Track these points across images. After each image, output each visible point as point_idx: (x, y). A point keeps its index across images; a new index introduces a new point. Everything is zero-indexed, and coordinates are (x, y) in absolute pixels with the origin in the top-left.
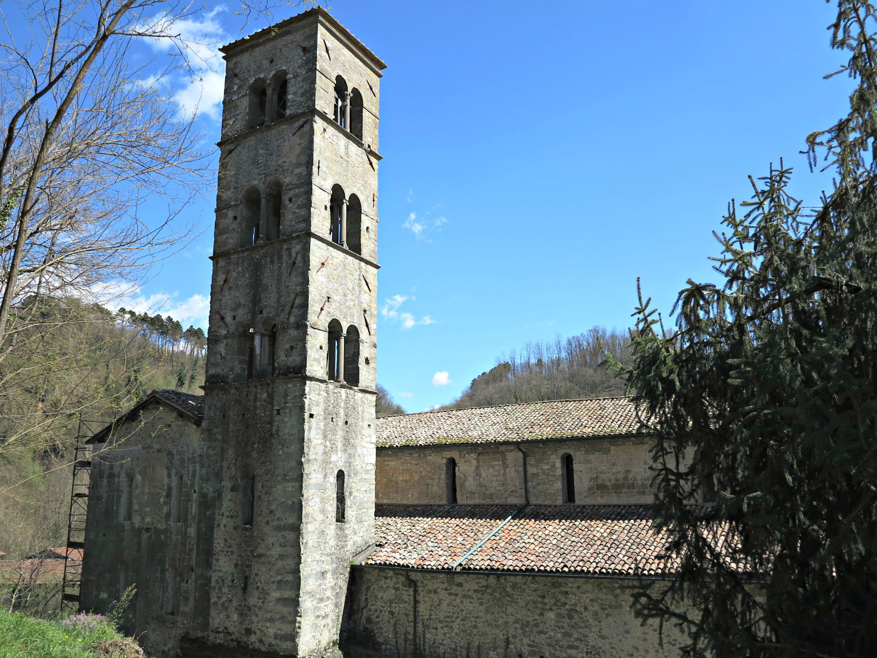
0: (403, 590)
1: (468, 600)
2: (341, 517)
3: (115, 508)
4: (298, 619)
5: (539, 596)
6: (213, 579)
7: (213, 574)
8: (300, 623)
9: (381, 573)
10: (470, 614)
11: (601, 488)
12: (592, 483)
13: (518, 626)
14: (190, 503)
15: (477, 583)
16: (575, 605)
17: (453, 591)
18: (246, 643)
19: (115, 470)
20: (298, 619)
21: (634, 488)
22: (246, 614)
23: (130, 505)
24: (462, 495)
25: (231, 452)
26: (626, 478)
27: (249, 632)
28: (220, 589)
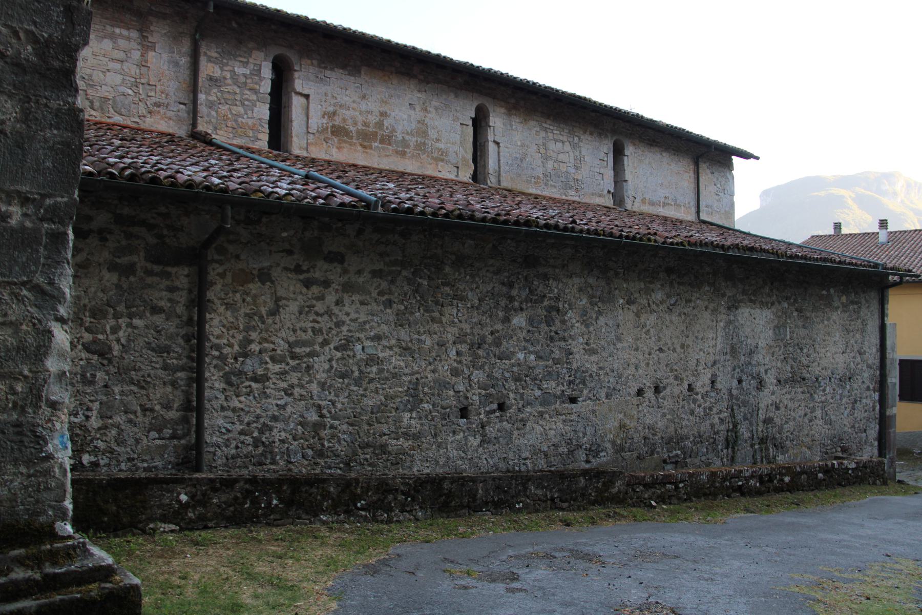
0: (149, 273)
1: (356, 297)
5: (503, 284)
10: (362, 329)
11: (339, 132)
12: (325, 121)
13: (464, 348)
15: (381, 255)
16: (557, 299)
17: (317, 275)
21: (390, 144)
26: (380, 125)
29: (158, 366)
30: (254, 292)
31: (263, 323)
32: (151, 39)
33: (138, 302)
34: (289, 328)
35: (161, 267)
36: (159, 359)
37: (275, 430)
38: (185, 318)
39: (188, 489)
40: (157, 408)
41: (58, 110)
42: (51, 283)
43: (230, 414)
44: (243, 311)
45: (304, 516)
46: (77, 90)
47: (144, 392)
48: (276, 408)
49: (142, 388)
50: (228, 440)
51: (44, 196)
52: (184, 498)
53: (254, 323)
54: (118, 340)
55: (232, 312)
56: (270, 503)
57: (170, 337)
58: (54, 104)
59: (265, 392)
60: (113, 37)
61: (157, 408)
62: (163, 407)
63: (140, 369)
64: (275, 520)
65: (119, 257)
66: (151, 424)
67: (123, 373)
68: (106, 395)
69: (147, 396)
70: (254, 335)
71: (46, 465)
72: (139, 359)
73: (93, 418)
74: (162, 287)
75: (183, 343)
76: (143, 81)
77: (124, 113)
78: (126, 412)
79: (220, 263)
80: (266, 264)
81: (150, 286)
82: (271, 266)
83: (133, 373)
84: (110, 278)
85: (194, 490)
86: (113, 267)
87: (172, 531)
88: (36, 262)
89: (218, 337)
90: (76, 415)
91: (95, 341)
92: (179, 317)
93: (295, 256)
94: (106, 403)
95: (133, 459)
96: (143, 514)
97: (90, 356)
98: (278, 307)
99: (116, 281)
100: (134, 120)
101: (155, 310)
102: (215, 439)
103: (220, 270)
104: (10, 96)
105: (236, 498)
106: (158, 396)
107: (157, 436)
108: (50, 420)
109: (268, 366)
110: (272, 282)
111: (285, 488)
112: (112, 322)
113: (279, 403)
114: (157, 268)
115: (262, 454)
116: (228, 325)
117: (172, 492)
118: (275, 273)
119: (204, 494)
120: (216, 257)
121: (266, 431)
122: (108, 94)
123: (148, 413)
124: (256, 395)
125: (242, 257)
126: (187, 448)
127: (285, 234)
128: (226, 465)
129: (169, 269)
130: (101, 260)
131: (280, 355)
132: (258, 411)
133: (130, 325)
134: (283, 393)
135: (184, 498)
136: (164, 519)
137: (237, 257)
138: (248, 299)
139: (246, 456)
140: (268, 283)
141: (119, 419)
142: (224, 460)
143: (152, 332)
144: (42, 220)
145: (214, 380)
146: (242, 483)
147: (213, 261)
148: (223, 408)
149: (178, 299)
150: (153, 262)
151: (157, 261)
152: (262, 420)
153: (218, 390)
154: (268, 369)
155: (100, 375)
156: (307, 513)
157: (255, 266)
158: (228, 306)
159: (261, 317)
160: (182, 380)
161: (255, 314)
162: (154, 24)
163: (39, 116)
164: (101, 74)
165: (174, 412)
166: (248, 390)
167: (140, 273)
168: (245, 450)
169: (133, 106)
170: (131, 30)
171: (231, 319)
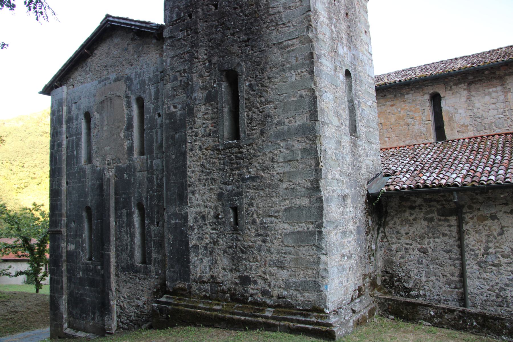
0: (440, 220)
2: (354, 130)
3: (75, 153)
4: (323, 257)
6: (190, 219)
7: (190, 211)
8: (326, 264)
9: (404, 203)
14: (154, 131)
18: (243, 295)
19: (72, 113)
20: (323, 257)
22: (239, 257)
23: (206, 309)
24: (452, 130)
25: (202, 54)
27: (245, 280)
28: (200, 228)
29: (447, 258)
30: (489, 225)
31: (495, 239)
32: (508, 87)
33: (436, 232)
34: (511, 241)
35: (444, 217)
36: (447, 255)
37: (508, 291)
38: (457, 238)
39: (434, 310)
40: (448, 275)
41: (317, 198)
42: (319, 245)
43: (482, 280)
44: (484, 234)
45: (491, 334)
46: (321, 191)
47: (442, 268)
48: (507, 280)
49: (441, 266)
50: (482, 292)
51: (316, 222)
52: (432, 313)
53: (491, 239)
54: (430, 247)
55: (479, 235)
56: (472, 324)
57: (451, 246)
58: (316, 197)
59: (500, 272)
60: (489, 94)
61: (448, 275)
62: (450, 275)
63: (439, 259)
64: (476, 332)
65: (427, 215)
66: (446, 281)
67: (433, 260)
68: (427, 268)
69: (444, 270)
70: (491, 245)
71: (321, 293)
72: (439, 255)
73: (423, 277)
74: (445, 225)
75: (457, 248)
76: (507, 109)
77: (501, 127)
78: (436, 276)
79: (471, 213)
80: (494, 211)
81: (441, 225)
82: (497, 212)
83: (437, 260)
84: (425, 223)
85: (436, 311)
86: (425, 219)
87: (429, 325)
88: (315, 239)
89: (473, 246)
90: (417, 275)
91: (422, 248)
92: (455, 237)
93: (510, 206)
94: (427, 272)
95: (439, 295)
96: (417, 316)
97: (420, 253)
98: (503, 231)
99: (427, 225)
100: (506, 129)
101: (444, 235)
102: (475, 291)
103: (471, 216)
104: (306, 197)
105: (455, 318)
106: (448, 270)
107: (449, 287)
108: (322, 281)
109: (500, 259)
110: (498, 219)
111: (480, 318)
112: (428, 240)
113: (508, 277)
114: (442, 218)
115: (501, 302)
116: (477, 240)
117: (427, 310)
118: (499, 215)
119: (441, 313)
120: (468, 211)
121: (502, 290)
122: (491, 121)
123: (444, 277)
124: (495, 273)
125: (481, 209)
126: (461, 293)
127: (502, 196)
128: (481, 304)
129: (448, 218)
130: (421, 217)
131: (506, 254)
132: (497, 281)
133: (434, 241)
134: (510, 273)
135: (432, 313)
136: (425, 320)
137: (479, 209)
138: (486, 228)
139: (492, 301)
140: (496, 220)
141: (433, 278)
142: (481, 301)
143: (444, 244)
144: (316, 228)
145: (471, 266)
146: (457, 312)
147: (467, 212)
148: (478, 278)
149: (453, 230)
150: (441, 216)
151: (443, 216)
152: (499, 285)
153: (476, 269)
154: (500, 261)
155: (424, 261)
156: (494, 333)
157: (488, 213)
158: (477, 232)
159: (494, 236)
160: (457, 264)
161: (490, 235)
162: (508, 79)
163: (313, 201)
164: (487, 113)
165: (456, 277)
166: (491, 270)
167: (436, 220)
168: (492, 298)
169: (504, 122)
170: (497, 87)
171: (479, 238)
